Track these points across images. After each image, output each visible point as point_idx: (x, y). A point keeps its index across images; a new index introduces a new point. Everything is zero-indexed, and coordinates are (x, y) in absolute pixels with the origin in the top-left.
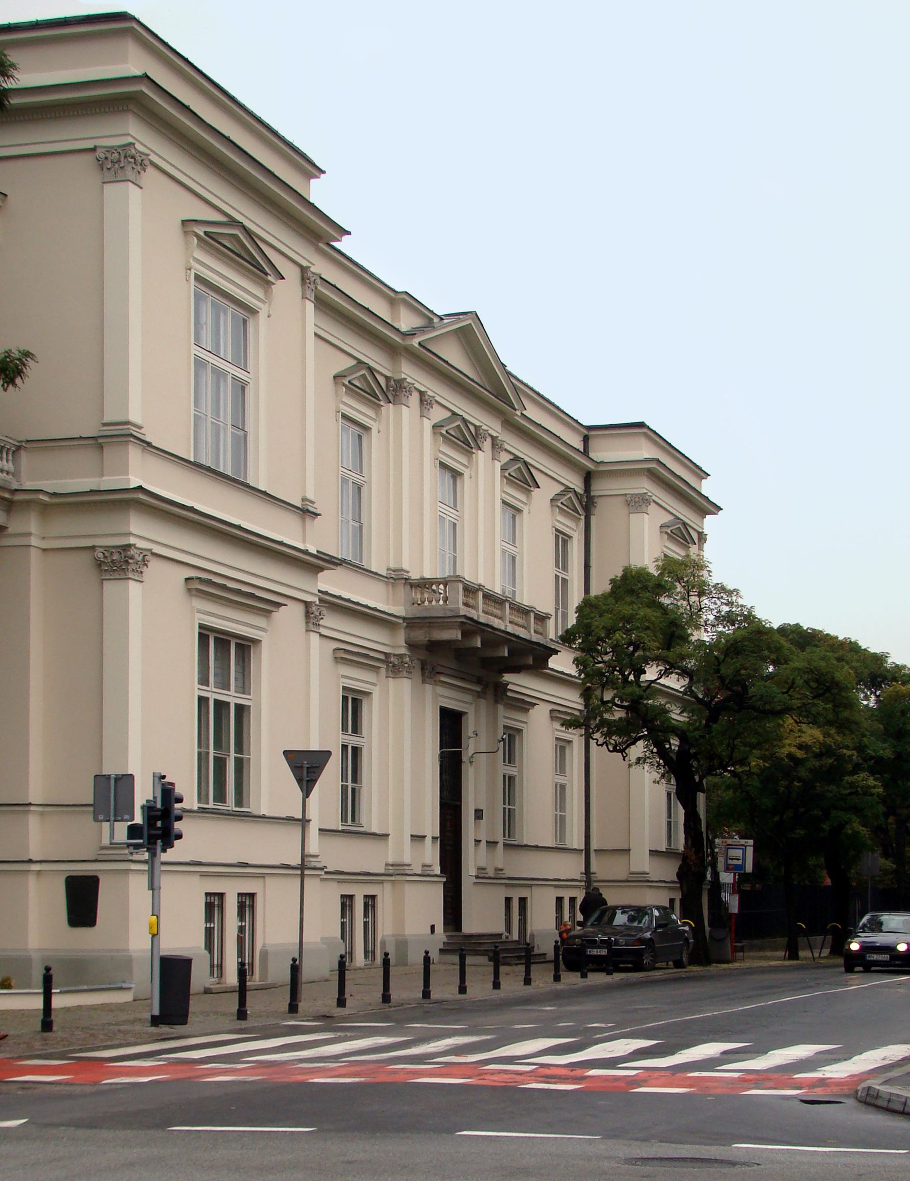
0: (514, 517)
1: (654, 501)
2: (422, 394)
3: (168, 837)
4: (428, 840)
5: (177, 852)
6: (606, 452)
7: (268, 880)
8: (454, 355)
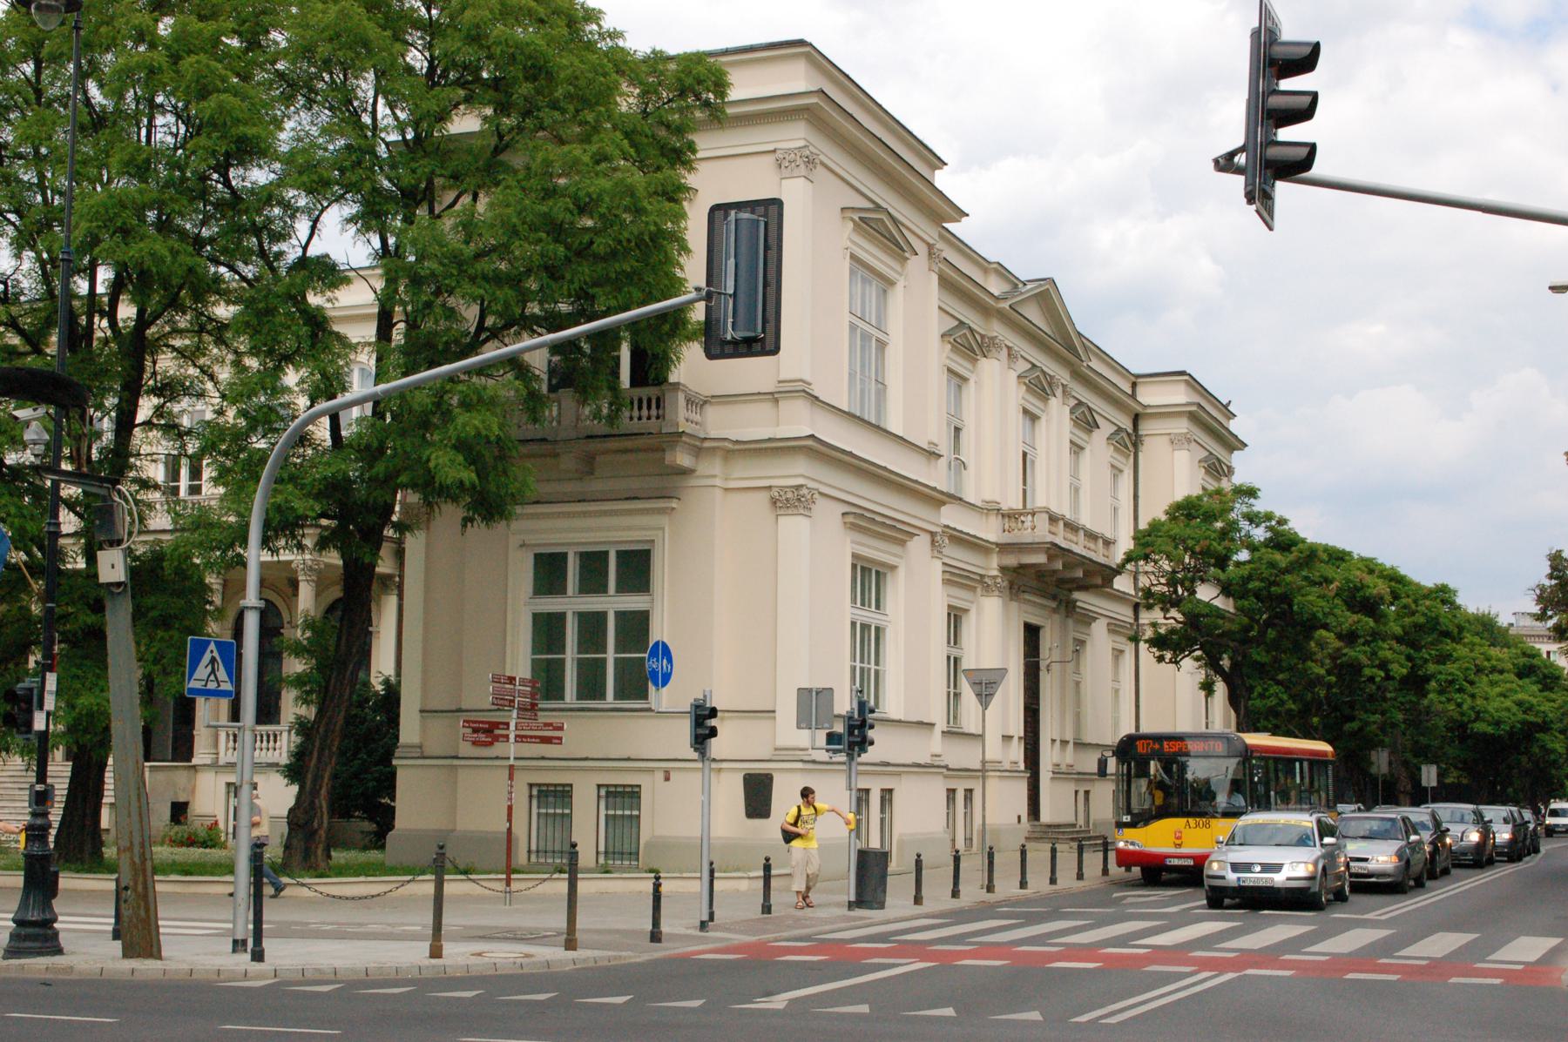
0: (960, 387)
1: (822, 163)
2: (1009, 348)
3: (863, 743)
4: (1016, 739)
5: (871, 754)
6: (1150, 396)
7: (904, 777)
8: (1034, 314)
